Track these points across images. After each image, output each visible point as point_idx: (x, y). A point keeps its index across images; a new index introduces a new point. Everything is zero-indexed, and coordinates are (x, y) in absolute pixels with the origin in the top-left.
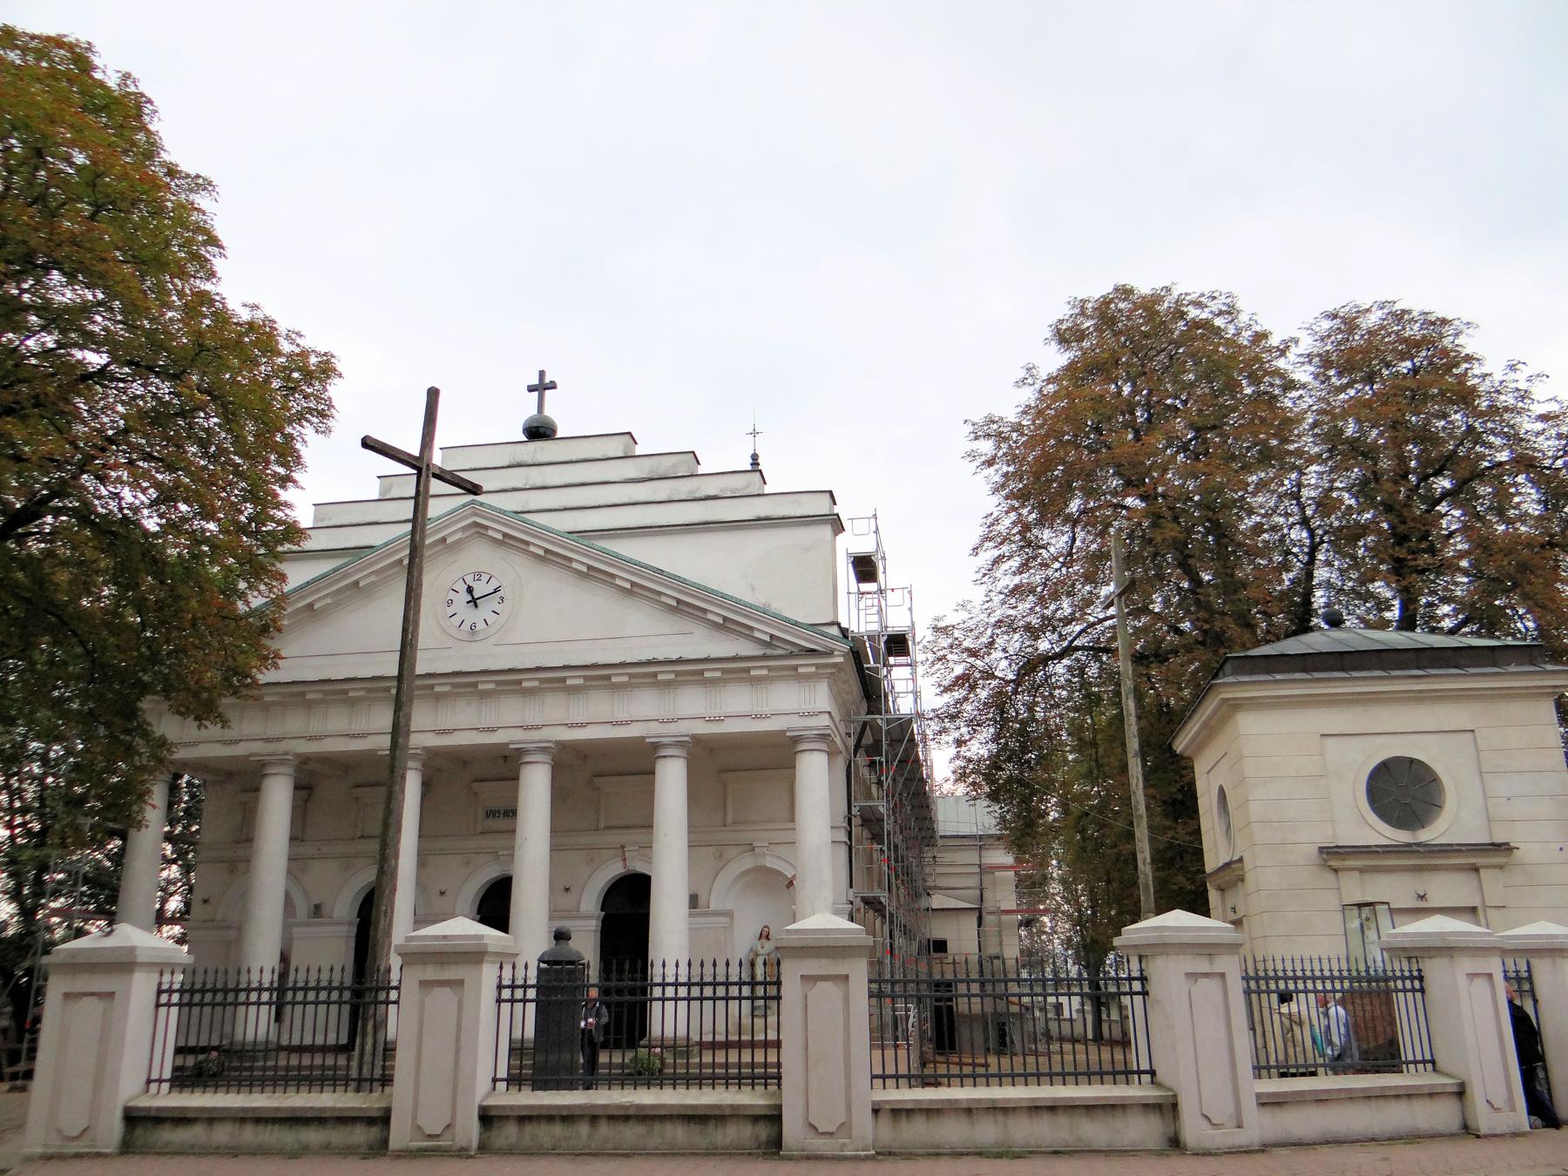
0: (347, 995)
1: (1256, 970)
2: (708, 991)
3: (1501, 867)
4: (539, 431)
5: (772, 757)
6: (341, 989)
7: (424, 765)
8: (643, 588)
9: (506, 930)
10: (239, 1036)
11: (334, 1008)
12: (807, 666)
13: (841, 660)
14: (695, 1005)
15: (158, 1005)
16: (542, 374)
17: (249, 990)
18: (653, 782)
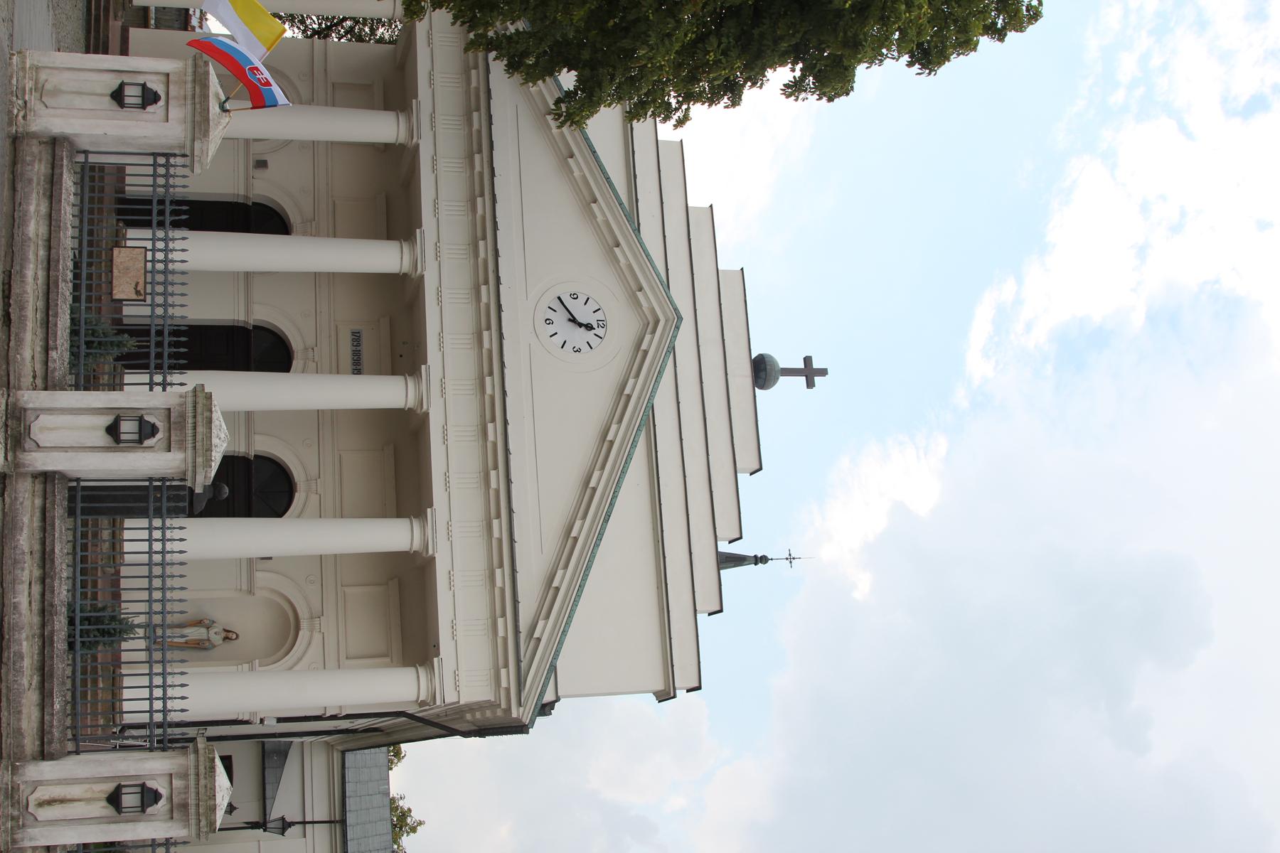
0: (158, 717)
1: (173, 589)
2: (158, 693)
4: (763, 372)
5: (415, 641)
6: (166, 186)
7: (405, 275)
8: (591, 504)
11: (145, 705)
12: (508, 678)
13: (514, 715)
14: (150, 170)
15: (155, 155)
16: (823, 372)
17: (164, 674)
18: (386, 374)
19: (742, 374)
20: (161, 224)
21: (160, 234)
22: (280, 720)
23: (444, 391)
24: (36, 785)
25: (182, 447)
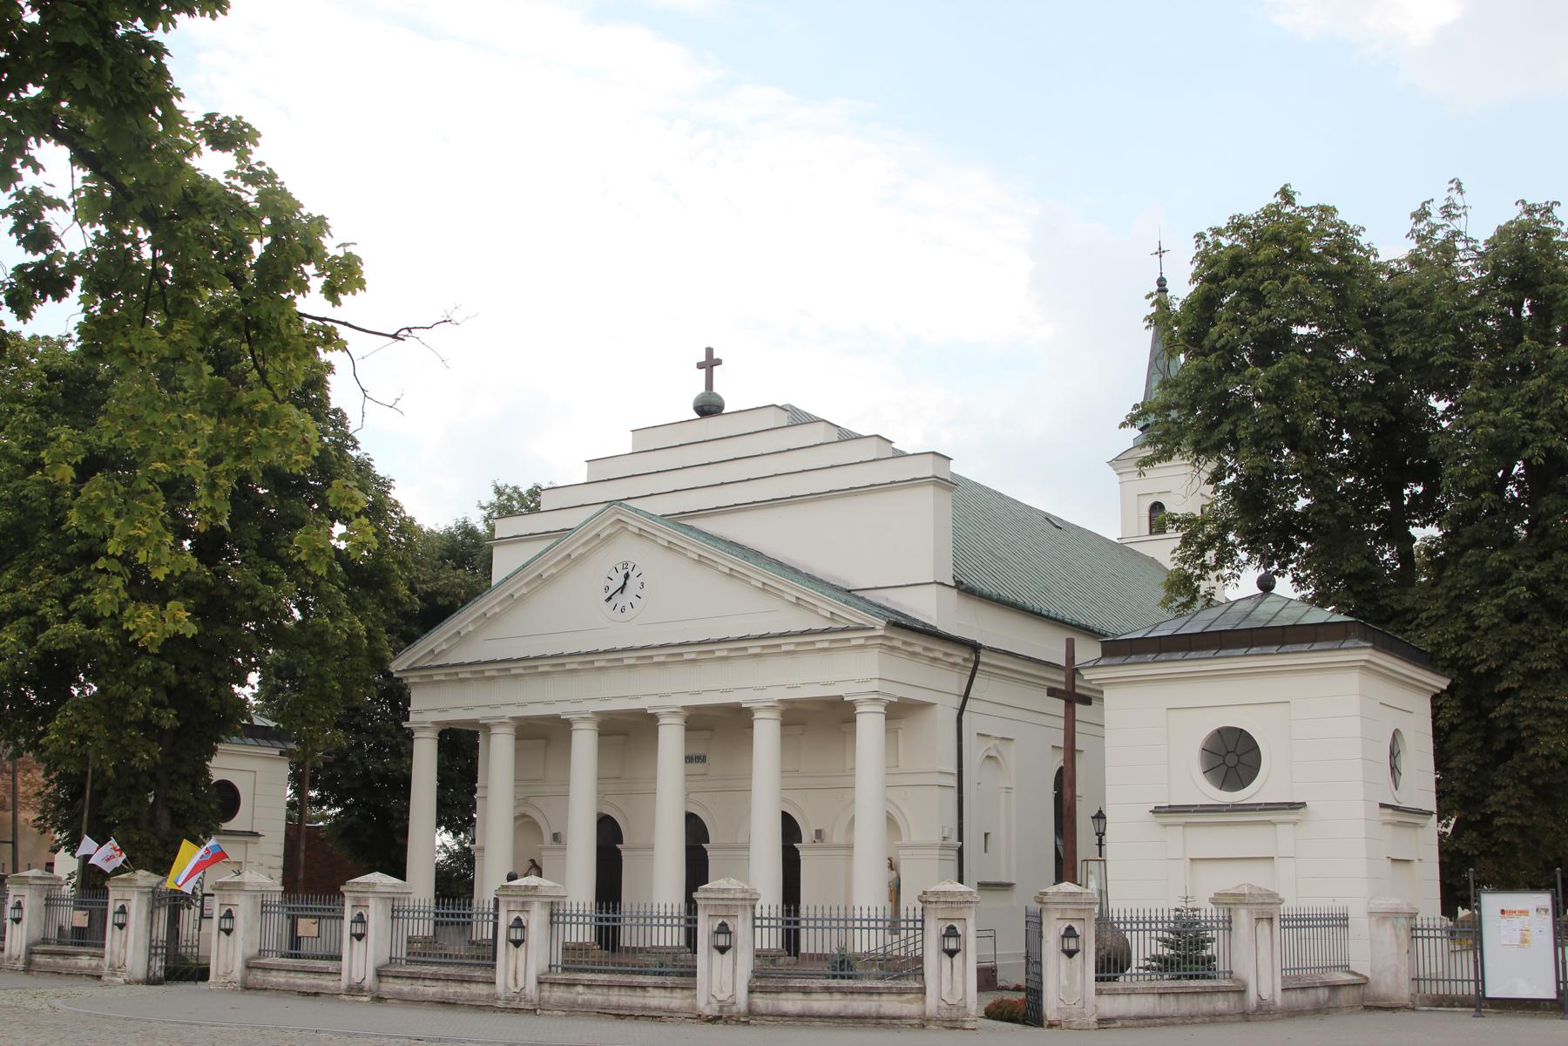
0: (683, 922)
2: (865, 924)
3: (1295, 823)
4: (708, 407)
9: (403, 877)
10: (850, 950)
12: (857, 638)
15: (754, 927)
16: (709, 351)
19: (712, 426)
20: (797, 923)
21: (803, 923)
22: (1100, 816)
23: (668, 693)
24: (506, 987)
25: (367, 899)
